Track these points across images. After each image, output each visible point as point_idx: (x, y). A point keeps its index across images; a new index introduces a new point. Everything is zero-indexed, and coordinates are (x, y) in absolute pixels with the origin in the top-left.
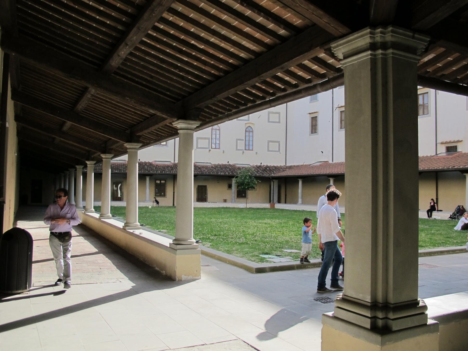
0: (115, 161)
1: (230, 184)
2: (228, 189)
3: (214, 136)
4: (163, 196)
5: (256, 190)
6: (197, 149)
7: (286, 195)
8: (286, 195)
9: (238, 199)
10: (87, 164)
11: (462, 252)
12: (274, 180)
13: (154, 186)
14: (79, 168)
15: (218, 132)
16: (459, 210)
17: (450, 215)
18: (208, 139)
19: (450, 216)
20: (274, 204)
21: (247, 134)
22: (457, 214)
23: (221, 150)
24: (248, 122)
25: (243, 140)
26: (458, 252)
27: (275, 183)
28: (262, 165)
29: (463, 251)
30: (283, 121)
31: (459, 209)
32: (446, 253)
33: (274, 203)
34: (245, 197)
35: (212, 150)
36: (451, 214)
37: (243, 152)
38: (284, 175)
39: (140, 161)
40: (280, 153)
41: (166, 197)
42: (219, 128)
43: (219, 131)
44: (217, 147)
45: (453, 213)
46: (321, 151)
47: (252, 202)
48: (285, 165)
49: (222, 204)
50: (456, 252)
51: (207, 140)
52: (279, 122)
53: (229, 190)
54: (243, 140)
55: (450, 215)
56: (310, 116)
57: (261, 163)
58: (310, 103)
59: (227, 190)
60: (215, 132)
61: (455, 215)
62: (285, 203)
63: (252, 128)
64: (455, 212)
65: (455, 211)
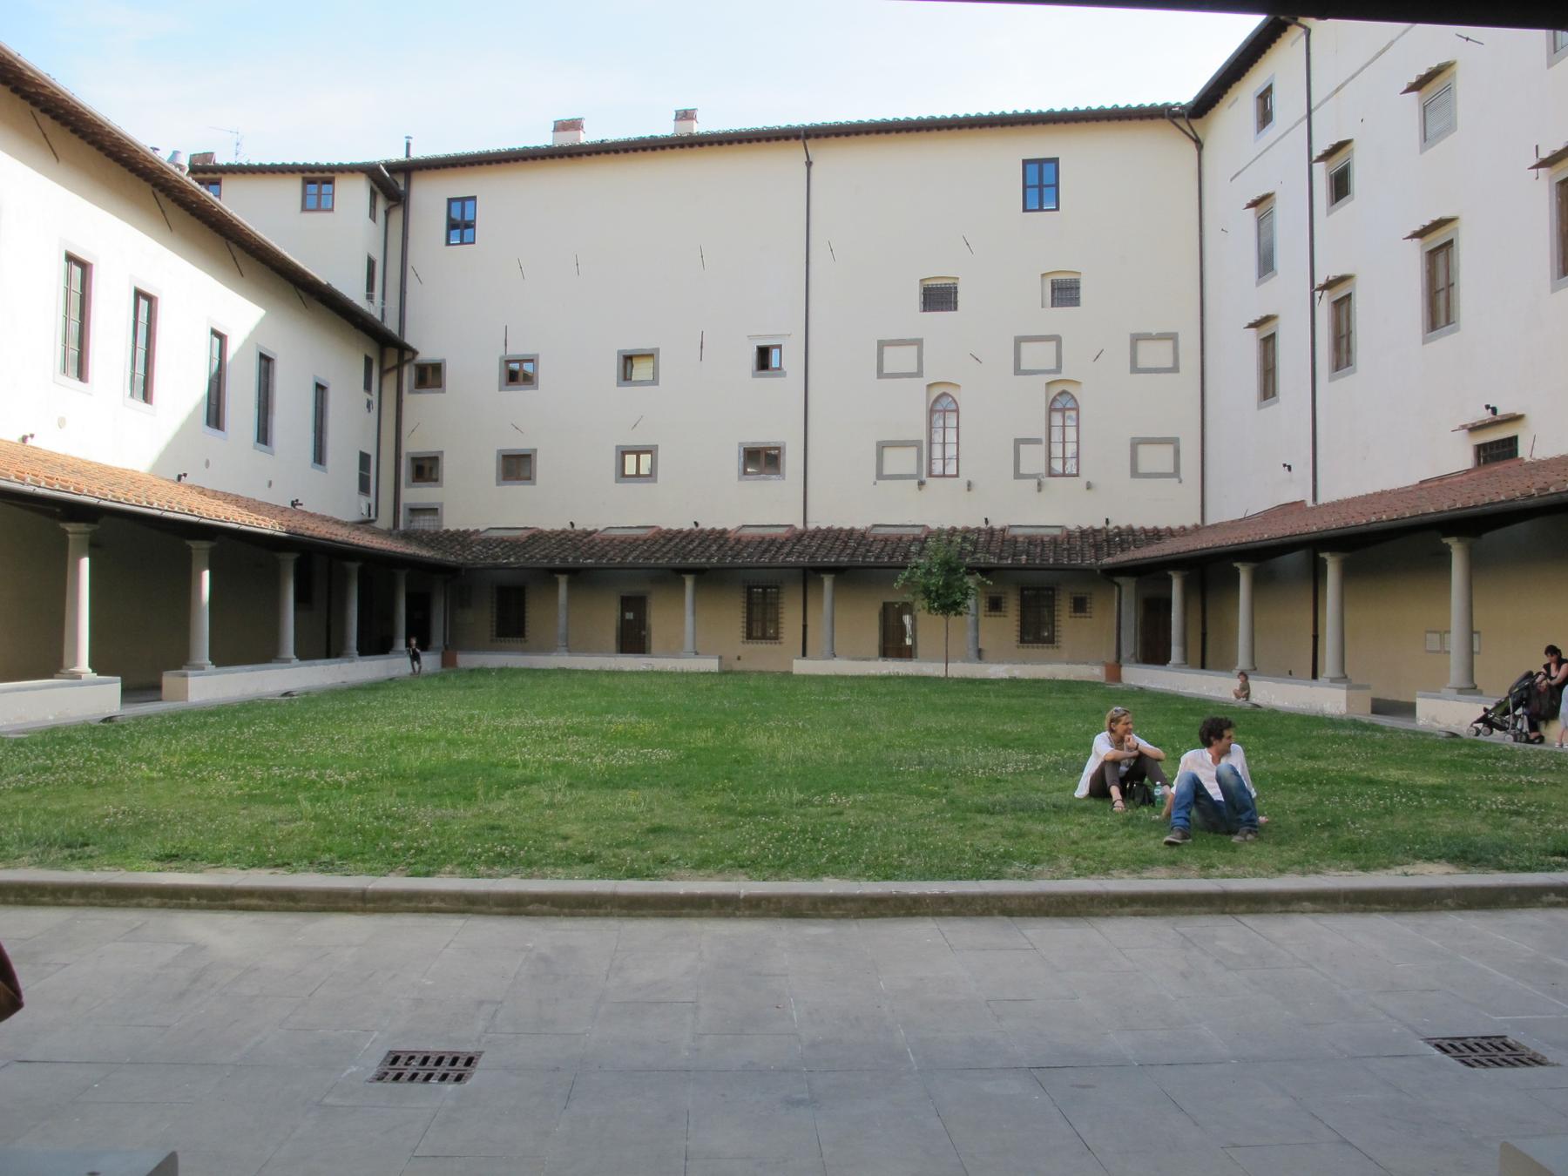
0: (620, 530)
1: (1079, 595)
2: (988, 613)
3: (938, 438)
4: (770, 639)
5: (1090, 617)
6: (879, 482)
7: (1204, 635)
8: (1204, 635)
9: (1023, 647)
10: (67, 532)
11: (292, 904)
12: (1121, 580)
13: (1017, 616)
14: (198, 549)
15: (952, 421)
16: (1529, 695)
17: (1485, 710)
18: (916, 444)
19: (1482, 713)
20: (1121, 666)
21: (1057, 419)
22: (1515, 710)
23: (963, 479)
24: (1058, 377)
25: (1037, 441)
26: (254, 902)
27: (1124, 590)
28: (1111, 526)
29: (302, 904)
30: (1190, 362)
31: (1527, 688)
32: (1307, 905)
33: (1122, 661)
34: (1051, 640)
35: (929, 481)
36: (1490, 707)
37: (1039, 484)
38: (1152, 554)
39: (700, 527)
40: (1180, 482)
41: (525, 641)
42: (953, 407)
43: (955, 414)
44: (951, 470)
45: (1498, 705)
46: (1285, 465)
47: (1072, 661)
48: (1199, 522)
49: (612, 659)
50: (237, 902)
51: (913, 450)
52: (1175, 369)
53: (990, 616)
54: (1037, 441)
55: (1485, 710)
56: (1258, 335)
57: (1107, 521)
58: (1258, 284)
59: (1070, 617)
60: (941, 422)
61: (1507, 712)
62: (1203, 666)
63: (1073, 397)
64: (1507, 698)
65: (1507, 695)
